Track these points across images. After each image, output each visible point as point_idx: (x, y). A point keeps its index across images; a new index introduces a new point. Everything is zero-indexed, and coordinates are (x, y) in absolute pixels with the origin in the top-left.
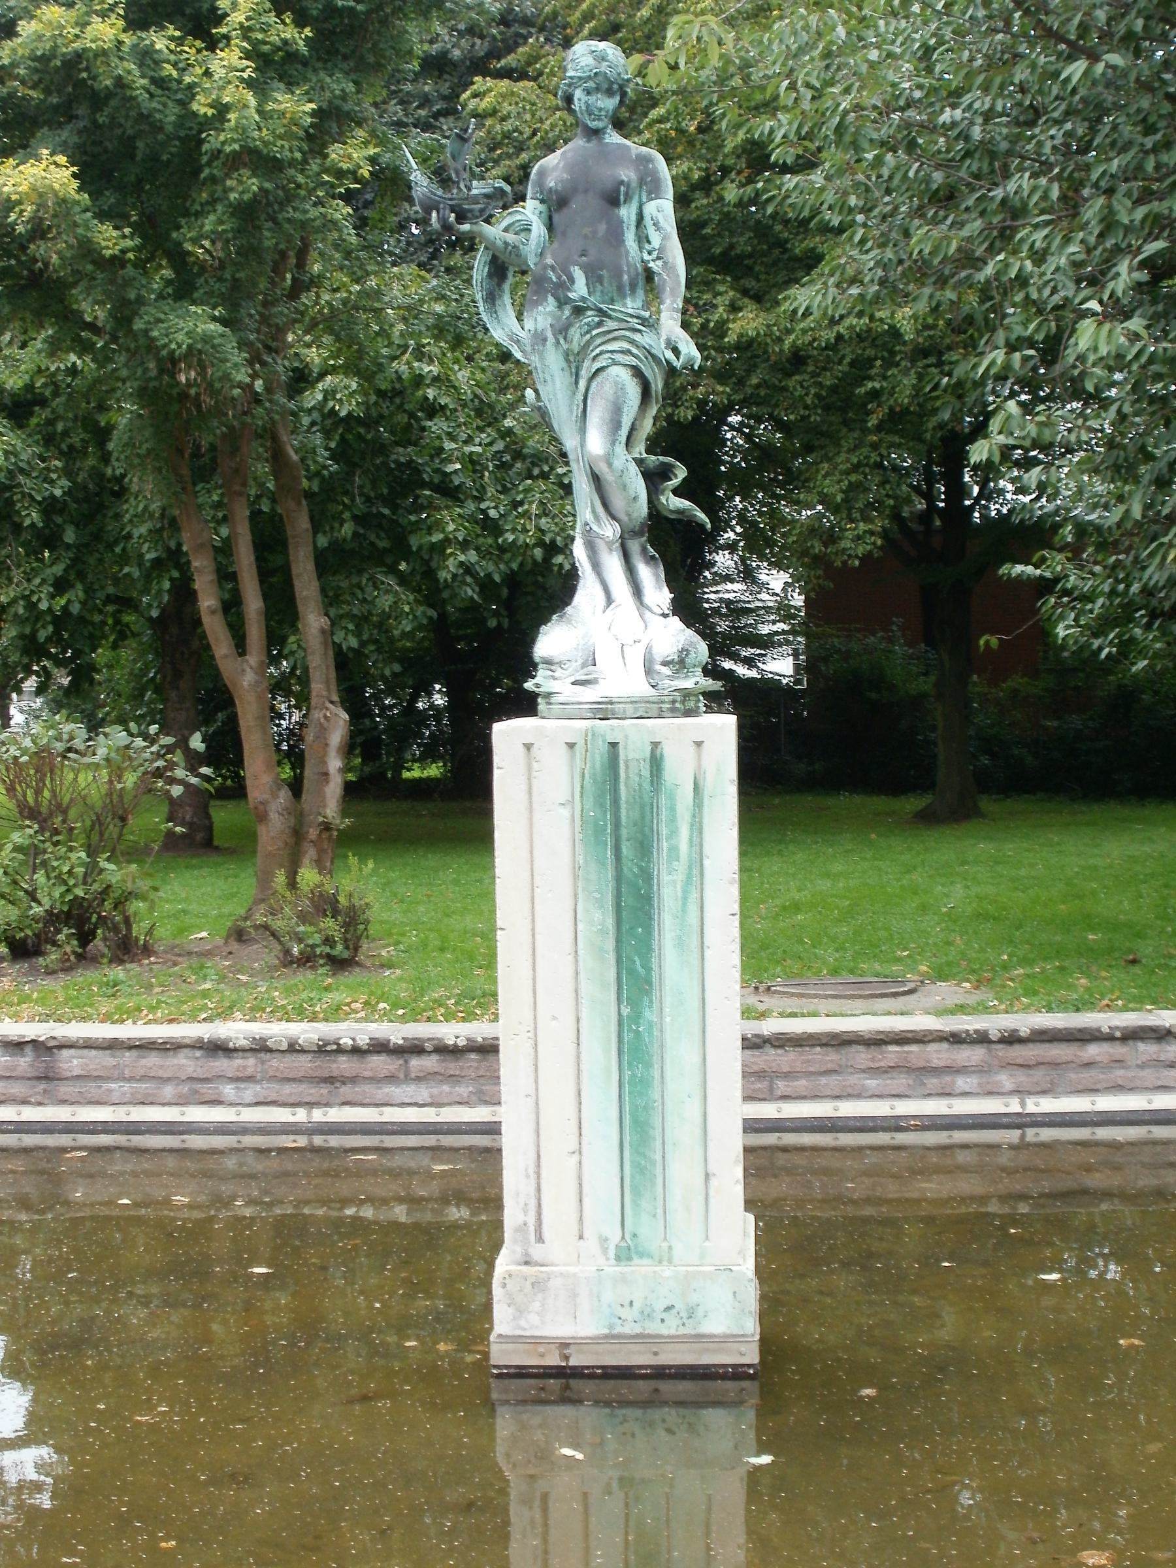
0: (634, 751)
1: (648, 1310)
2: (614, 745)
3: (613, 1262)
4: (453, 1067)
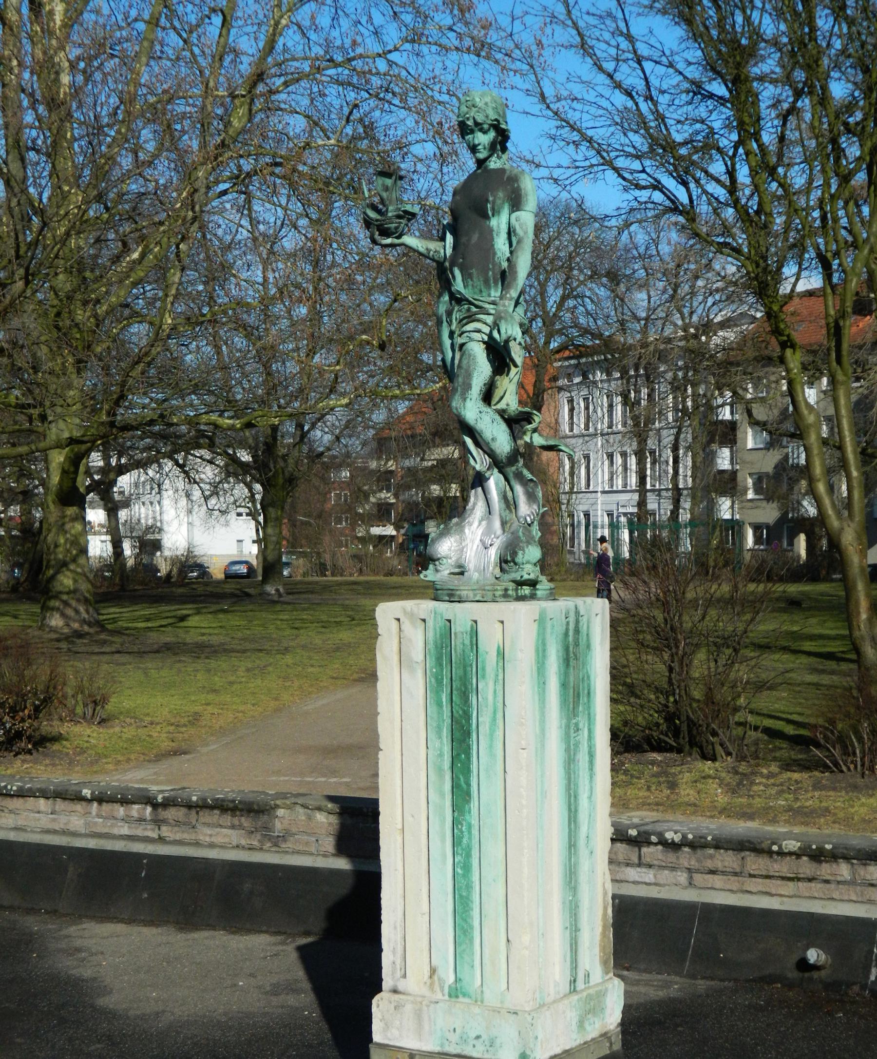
0: (461, 626)
1: (465, 1037)
2: (449, 621)
3: (447, 997)
4: (671, 857)
